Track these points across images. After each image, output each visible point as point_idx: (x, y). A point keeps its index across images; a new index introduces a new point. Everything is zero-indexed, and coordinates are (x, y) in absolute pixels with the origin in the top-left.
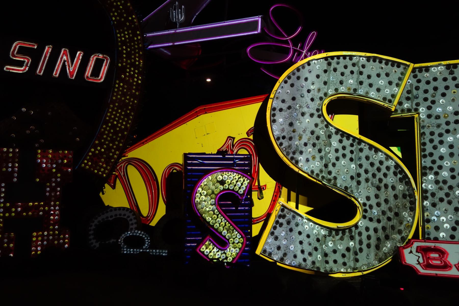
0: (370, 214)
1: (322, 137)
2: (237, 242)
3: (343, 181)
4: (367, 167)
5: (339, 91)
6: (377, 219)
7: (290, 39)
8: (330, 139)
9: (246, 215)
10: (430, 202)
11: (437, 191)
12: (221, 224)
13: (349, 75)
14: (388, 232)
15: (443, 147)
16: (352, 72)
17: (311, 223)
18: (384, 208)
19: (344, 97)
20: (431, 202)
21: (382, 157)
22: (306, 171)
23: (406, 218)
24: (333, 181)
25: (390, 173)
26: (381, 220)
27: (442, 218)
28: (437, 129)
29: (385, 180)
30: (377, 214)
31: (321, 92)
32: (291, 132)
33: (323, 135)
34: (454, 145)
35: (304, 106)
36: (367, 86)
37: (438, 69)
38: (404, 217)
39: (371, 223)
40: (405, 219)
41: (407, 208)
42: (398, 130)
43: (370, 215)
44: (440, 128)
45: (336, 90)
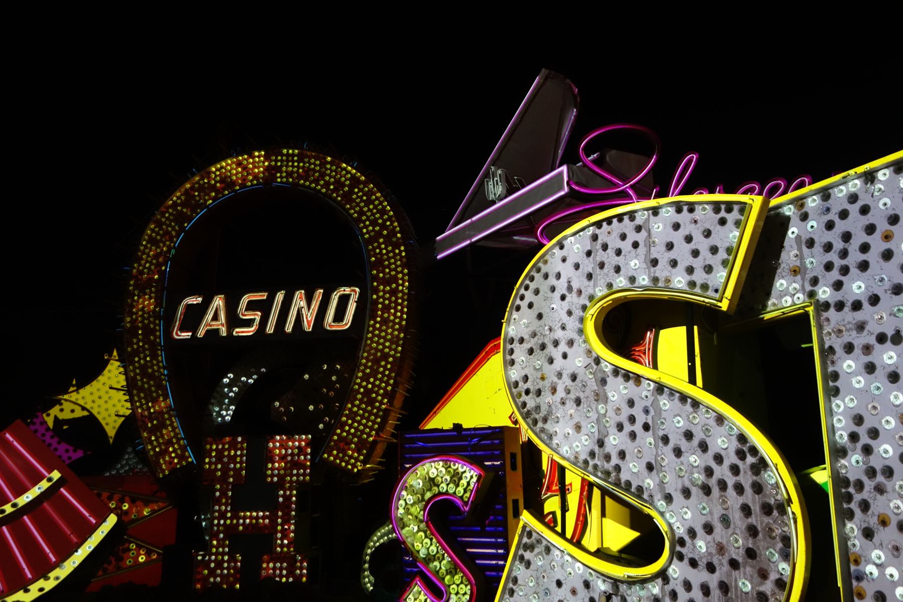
0: (691, 551)
1: (590, 383)
2: (463, 592)
3: (631, 475)
4: (678, 443)
5: (615, 288)
6: (706, 563)
7: (632, 187)
8: (605, 388)
9: (500, 542)
10: (859, 526)
11: (871, 495)
12: (437, 556)
13: (630, 252)
14: (734, 597)
15: (876, 380)
16: (636, 245)
17: (578, 564)
18: (722, 537)
19: (625, 297)
20: (861, 525)
21: (709, 416)
22: (567, 455)
23: (776, 564)
24: (613, 475)
25: (728, 454)
26: (716, 566)
27: (890, 570)
28: (858, 335)
29: (720, 471)
30: (707, 551)
31: (583, 295)
32: (538, 380)
33: (591, 380)
34: (899, 371)
35: (557, 327)
36: (666, 267)
37: (847, 188)
38: (769, 560)
39: (695, 571)
40: (773, 567)
41: (774, 538)
42: (803, 346)
43: (691, 552)
44: (865, 332)
45: (610, 286)
